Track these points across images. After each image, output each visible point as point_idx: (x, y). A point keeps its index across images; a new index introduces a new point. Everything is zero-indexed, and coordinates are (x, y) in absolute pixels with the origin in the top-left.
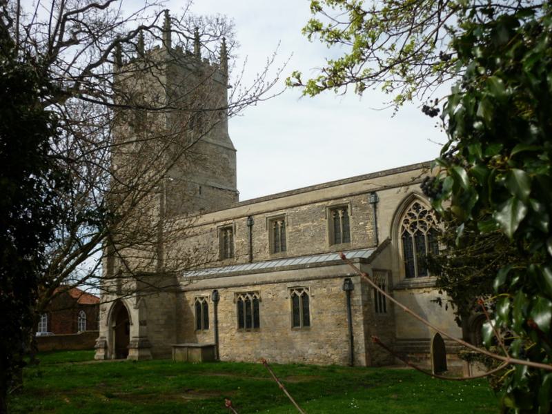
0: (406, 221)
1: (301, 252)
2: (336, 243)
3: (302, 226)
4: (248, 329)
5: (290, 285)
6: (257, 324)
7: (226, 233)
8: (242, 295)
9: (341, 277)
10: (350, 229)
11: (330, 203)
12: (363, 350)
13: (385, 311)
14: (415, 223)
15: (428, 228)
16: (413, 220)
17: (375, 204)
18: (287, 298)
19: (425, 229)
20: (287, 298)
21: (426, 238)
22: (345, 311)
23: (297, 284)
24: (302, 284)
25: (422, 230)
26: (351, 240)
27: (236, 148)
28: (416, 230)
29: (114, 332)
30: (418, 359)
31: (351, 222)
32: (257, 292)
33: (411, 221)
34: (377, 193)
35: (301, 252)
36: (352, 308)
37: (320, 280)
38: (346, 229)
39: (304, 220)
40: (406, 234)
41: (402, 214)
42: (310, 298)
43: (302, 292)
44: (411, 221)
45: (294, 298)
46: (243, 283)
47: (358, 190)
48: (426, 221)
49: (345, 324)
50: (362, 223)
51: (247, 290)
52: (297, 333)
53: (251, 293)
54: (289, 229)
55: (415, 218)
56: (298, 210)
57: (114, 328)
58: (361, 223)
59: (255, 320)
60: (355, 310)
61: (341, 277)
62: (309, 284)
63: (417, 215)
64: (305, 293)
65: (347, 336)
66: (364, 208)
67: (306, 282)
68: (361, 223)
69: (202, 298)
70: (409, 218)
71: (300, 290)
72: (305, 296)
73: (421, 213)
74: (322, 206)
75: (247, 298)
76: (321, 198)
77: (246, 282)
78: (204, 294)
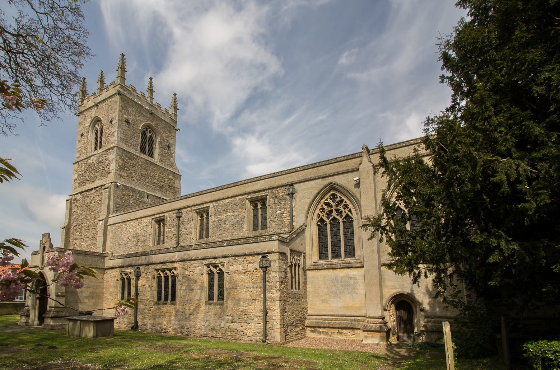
0: (322, 210)
1: (223, 237)
2: (254, 230)
3: (222, 217)
4: (172, 302)
5: (207, 262)
6: (173, 298)
7: (160, 225)
8: (162, 271)
9: (258, 254)
10: (268, 217)
11: (250, 196)
12: (279, 326)
13: (299, 289)
14: (331, 212)
15: (344, 215)
16: (329, 209)
17: (292, 195)
18: (202, 274)
19: (341, 216)
20: (202, 274)
21: (341, 224)
22: (260, 288)
23: (213, 261)
24: (218, 261)
25: (338, 217)
26: (268, 226)
27: (126, 78)
28: (331, 218)
29: (38, 302)
30: (330, 333)
31: (269, 211)
32: (175, 269)
33: (327, 209)
34: (295, 185)
35: (223, 237)
36: (268, 284)
37: (236, 258)
38: (264, 219)
39: (226, 211)
40: (322, 220)
41: (319, 203)
42: (225, 274)
43: (218, 268)
44: (327, 209)
45: (211, 274)
46: (163, 261)
47: (276, 184)
48: (342, 209)
49: (260, 299)
50: (280, 212)
51: (165, 267)
52: (210, 307)
53: (170, 270)
54: (212, 219)
55: (331, 207)
56: (221, 203)
57: (37, 298)
58: (278, 212)
59: (172, 295)
60: (271, 286)
61: (258, 254)
62: (225, 261)
63: (333, 204)
64: (220, 270)
65: (261, 311)
66: (281, 199)
67: (222, 259)
68: (278, 212)
69: (126, 274)
70: (324, 206)
71: (216, 267)
72: (221, 273)
73: (338, 202)
74: (243, 200)
75: (166, 274)
76: (242, 192)
77: (166, 260)
78: (127, 270)
